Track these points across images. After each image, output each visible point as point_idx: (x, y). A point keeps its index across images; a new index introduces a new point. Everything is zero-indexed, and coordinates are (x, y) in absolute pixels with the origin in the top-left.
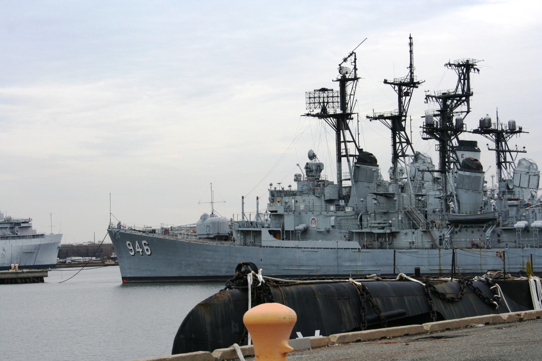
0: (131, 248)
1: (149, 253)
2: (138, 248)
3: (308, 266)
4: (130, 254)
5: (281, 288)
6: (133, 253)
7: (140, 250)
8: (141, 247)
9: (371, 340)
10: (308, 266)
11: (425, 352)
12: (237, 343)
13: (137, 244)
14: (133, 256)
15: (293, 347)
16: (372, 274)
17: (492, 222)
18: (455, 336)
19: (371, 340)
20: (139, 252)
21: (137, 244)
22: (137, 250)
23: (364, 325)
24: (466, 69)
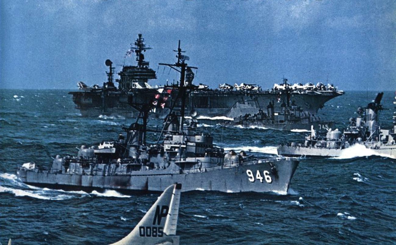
0: (252, 175)
1: (270, 181)
2: (259, 176)
3: (75, 117)
4: (249, 181)
5: (181, 141)
6: (253, 180)
7: (261, 178)
8: (262, 175)
9: (290, 218)
10: (75, 117)
11: (165, 139)
12: (93, 190)
13: (258, 173)
14: (253, 183)
15: (142, 134)
16: (333, 157)
17: (312, 136)
18: (335, 174)
19: (290, 218)
20: (259, 180)
21: (258, 173)
22: (257, 178)
23: (162, 137)
24: (292, 129)
